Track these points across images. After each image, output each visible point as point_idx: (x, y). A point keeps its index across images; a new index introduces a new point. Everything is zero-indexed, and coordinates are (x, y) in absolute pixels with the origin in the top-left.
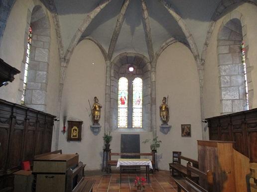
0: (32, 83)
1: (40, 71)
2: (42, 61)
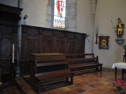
0: (67, 17)
1: (71, 9)
2: (71, 3)
